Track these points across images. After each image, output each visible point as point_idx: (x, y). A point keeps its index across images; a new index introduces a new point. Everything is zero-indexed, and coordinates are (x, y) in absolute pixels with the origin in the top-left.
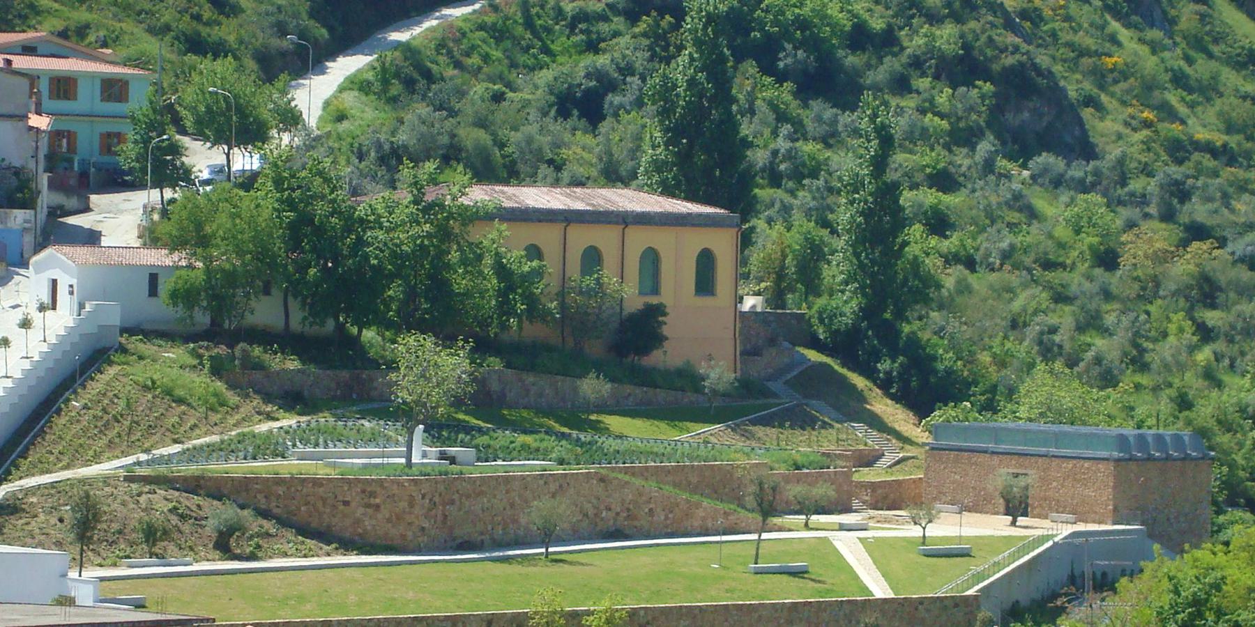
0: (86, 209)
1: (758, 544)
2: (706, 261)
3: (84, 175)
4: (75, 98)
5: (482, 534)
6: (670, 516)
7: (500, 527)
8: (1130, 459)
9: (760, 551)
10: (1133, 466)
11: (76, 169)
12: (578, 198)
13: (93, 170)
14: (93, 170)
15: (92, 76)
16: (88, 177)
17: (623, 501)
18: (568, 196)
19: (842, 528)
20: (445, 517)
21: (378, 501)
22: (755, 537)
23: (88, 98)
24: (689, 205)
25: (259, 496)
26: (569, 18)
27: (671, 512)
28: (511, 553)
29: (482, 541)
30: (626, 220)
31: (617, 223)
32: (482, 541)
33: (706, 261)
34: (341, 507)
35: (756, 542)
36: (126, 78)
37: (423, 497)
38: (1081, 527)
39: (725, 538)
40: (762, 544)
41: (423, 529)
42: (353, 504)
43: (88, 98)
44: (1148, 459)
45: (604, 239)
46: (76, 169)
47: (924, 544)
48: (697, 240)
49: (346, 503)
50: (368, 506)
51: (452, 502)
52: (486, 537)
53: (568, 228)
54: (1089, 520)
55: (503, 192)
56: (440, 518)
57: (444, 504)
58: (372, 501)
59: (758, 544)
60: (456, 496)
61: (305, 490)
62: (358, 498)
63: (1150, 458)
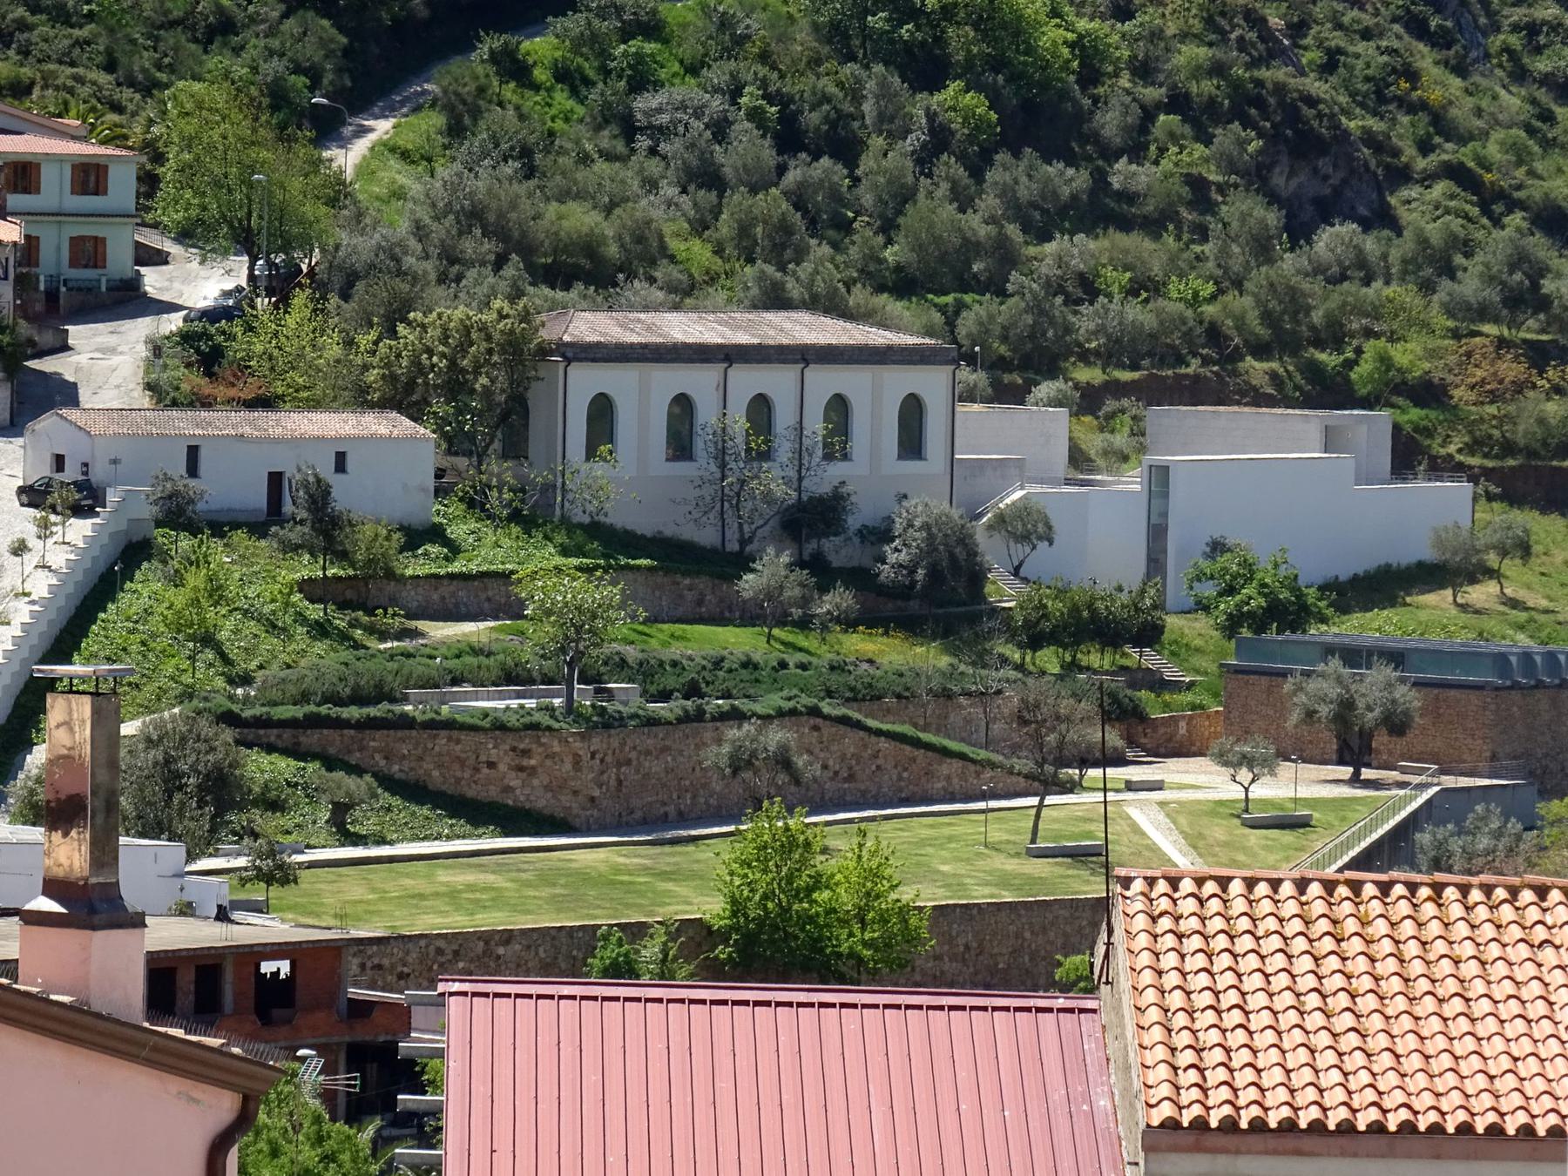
0: (65, 348)
1: (1038, 816)
2: (912, 411)
3: (52, 296)
4: (38, 191)
5: (664, 804)
6: (905, 775)
7: (689, 796)
8: (1511, 688)
9: (1041, 826)
10: (1516, 695)
11: (42, 287)
12: (739, 327)
13: (63, 289)
14: (63, 289)
15: (59, 159)
16: (58, 298)
17: (843, 758)
18: (726, 324)
19: (1130, 786)
20: (620, 782)
21: (533, 762)
22: (1034, 801)
23: (54, 189)
24: (888, 334)
25: (377, 757)
26: (484, 50)
27: (906, 769)
28: (694, 833)
29: (666, 815)
30: (805, 356)
31: (796, 362)
32: (666, 815)
33: (912, 411)
34: (485, 771)
35: (1033, 811)
36: (102, 161)
37: (593, 757)
38: (1450, 781)
39: (993, 804)
40: (1044, 812)
41: (593, 799)
42: (502, 767)
43: (54, 189)
44: (1536, 687)
45: (777, 382)
46: (42, 287)
47: (1246, 811)
48: (901, 381)
49: (491, 765)
50: (521, 769)
51: (628, 762)
52: (671, 809)
53: (730, 371)
54: (1374, 763)
55: (639, 321)
56: (613, 783)
57: (619, 765)
58: (525, 762)
59: (1038, 816)
60: (633, 755)
61: (437, 748)
62: (507, 759)
63: (1539, 685)
